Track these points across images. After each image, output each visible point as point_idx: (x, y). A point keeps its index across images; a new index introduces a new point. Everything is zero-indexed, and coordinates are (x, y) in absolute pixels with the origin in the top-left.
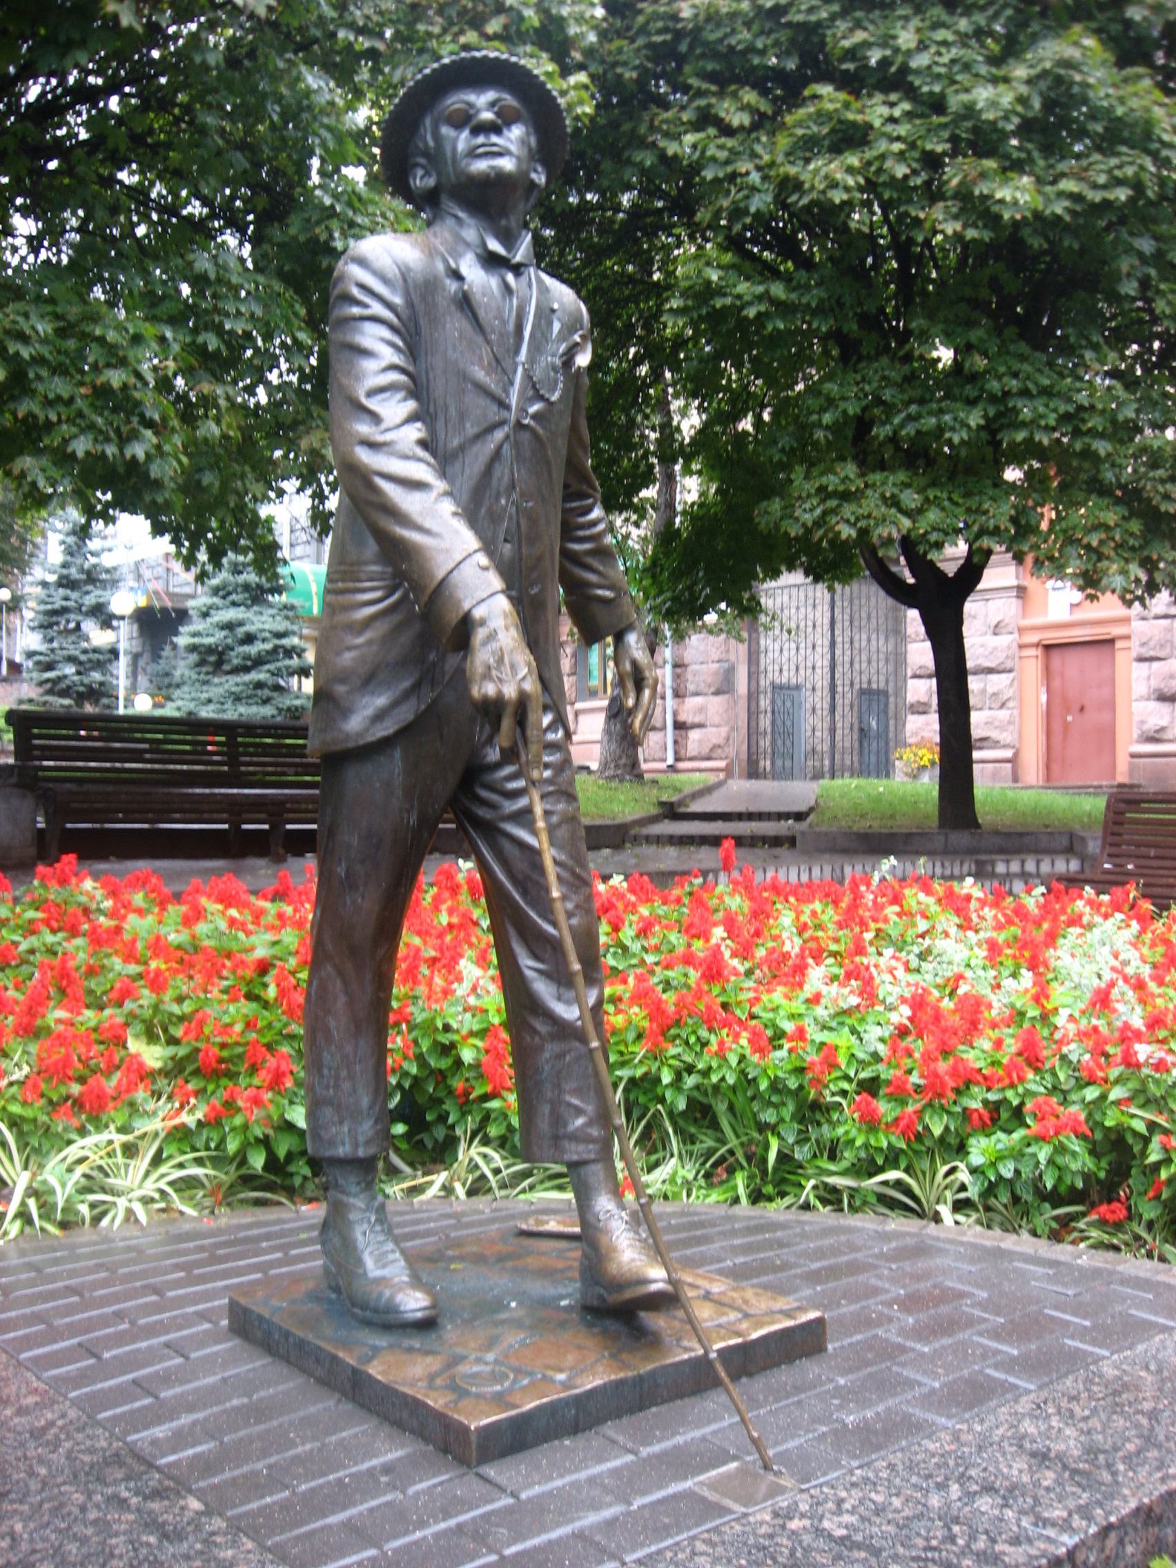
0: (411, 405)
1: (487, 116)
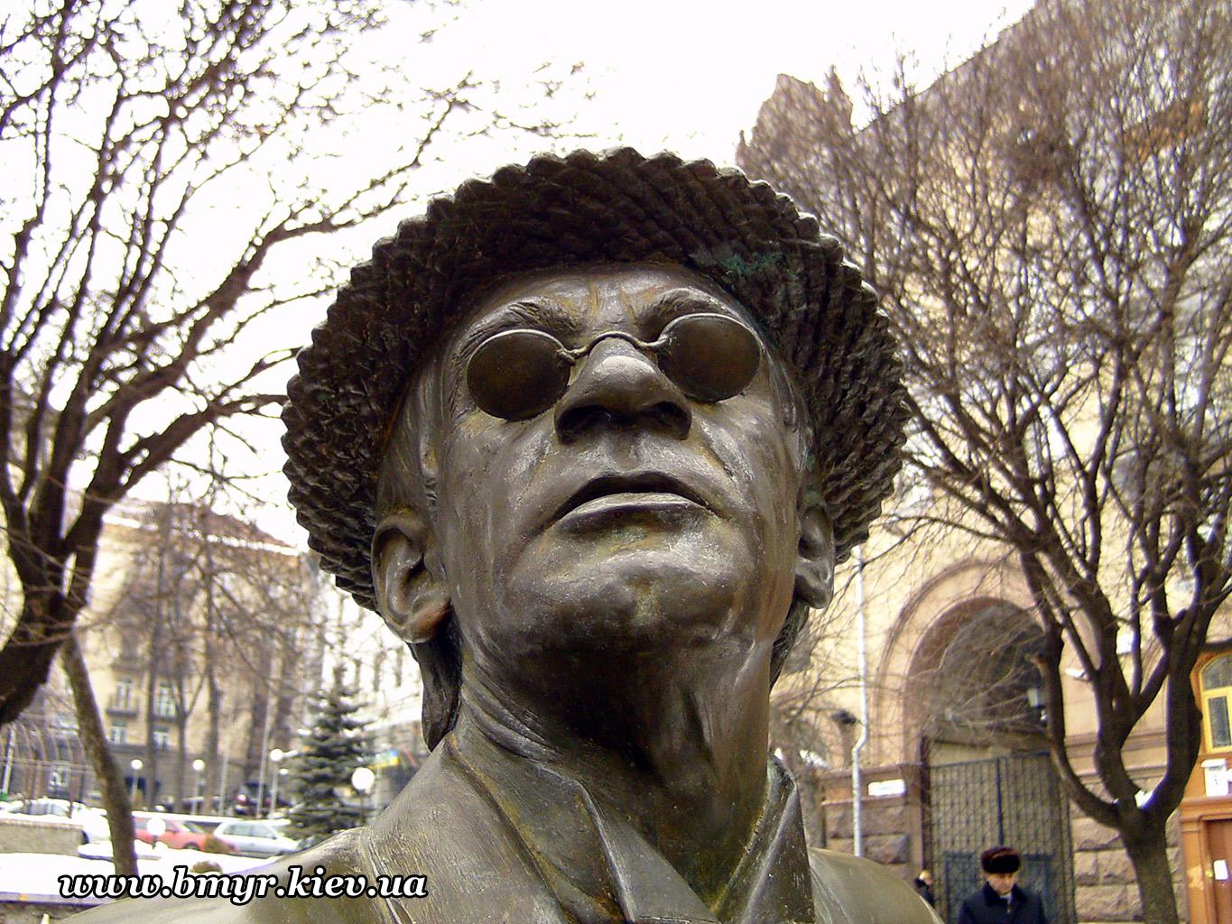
1: (622, 362)
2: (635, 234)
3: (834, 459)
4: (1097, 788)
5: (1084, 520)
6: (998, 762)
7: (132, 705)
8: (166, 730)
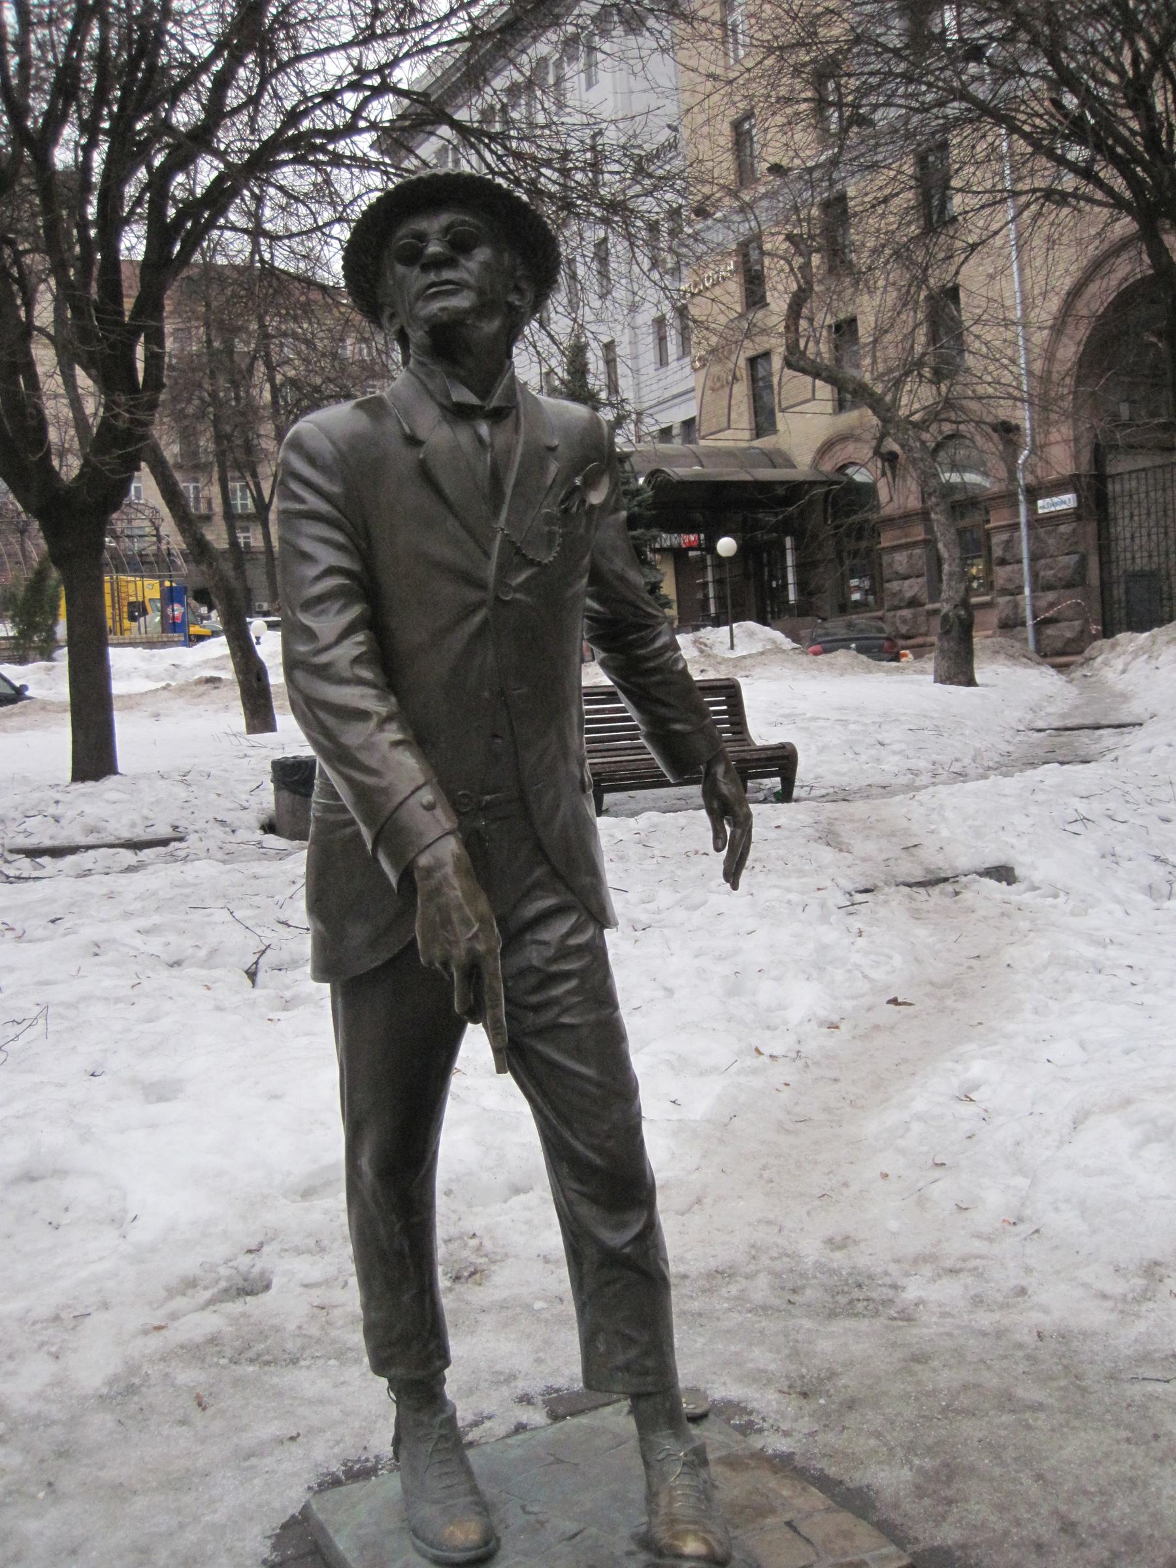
0: (355, 611)
1: (433, 248)
8: (246, 530)
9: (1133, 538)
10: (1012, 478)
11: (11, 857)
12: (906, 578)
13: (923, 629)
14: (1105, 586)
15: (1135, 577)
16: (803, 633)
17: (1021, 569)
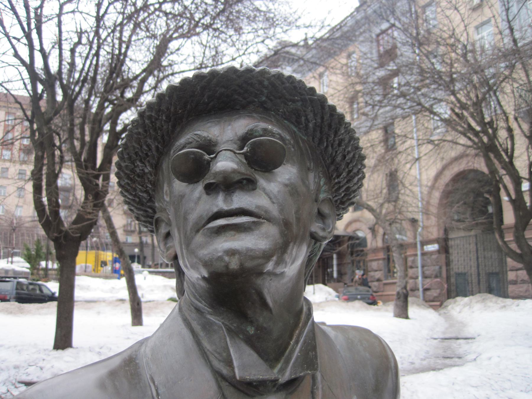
1: (225, 163)
2: (241, 99)
3: (336, 176)
4: (513, 246)
5: (507, 138)
6: (476, 236)
7: (133, 229)
9: (458, 261)
10: (415, 238)
11: (18, 385)
12: (376, 271)
13: (382, 290)
14: (448, 278)
15: (458, 275)
16: (340, 290)
17: (418, 271)
